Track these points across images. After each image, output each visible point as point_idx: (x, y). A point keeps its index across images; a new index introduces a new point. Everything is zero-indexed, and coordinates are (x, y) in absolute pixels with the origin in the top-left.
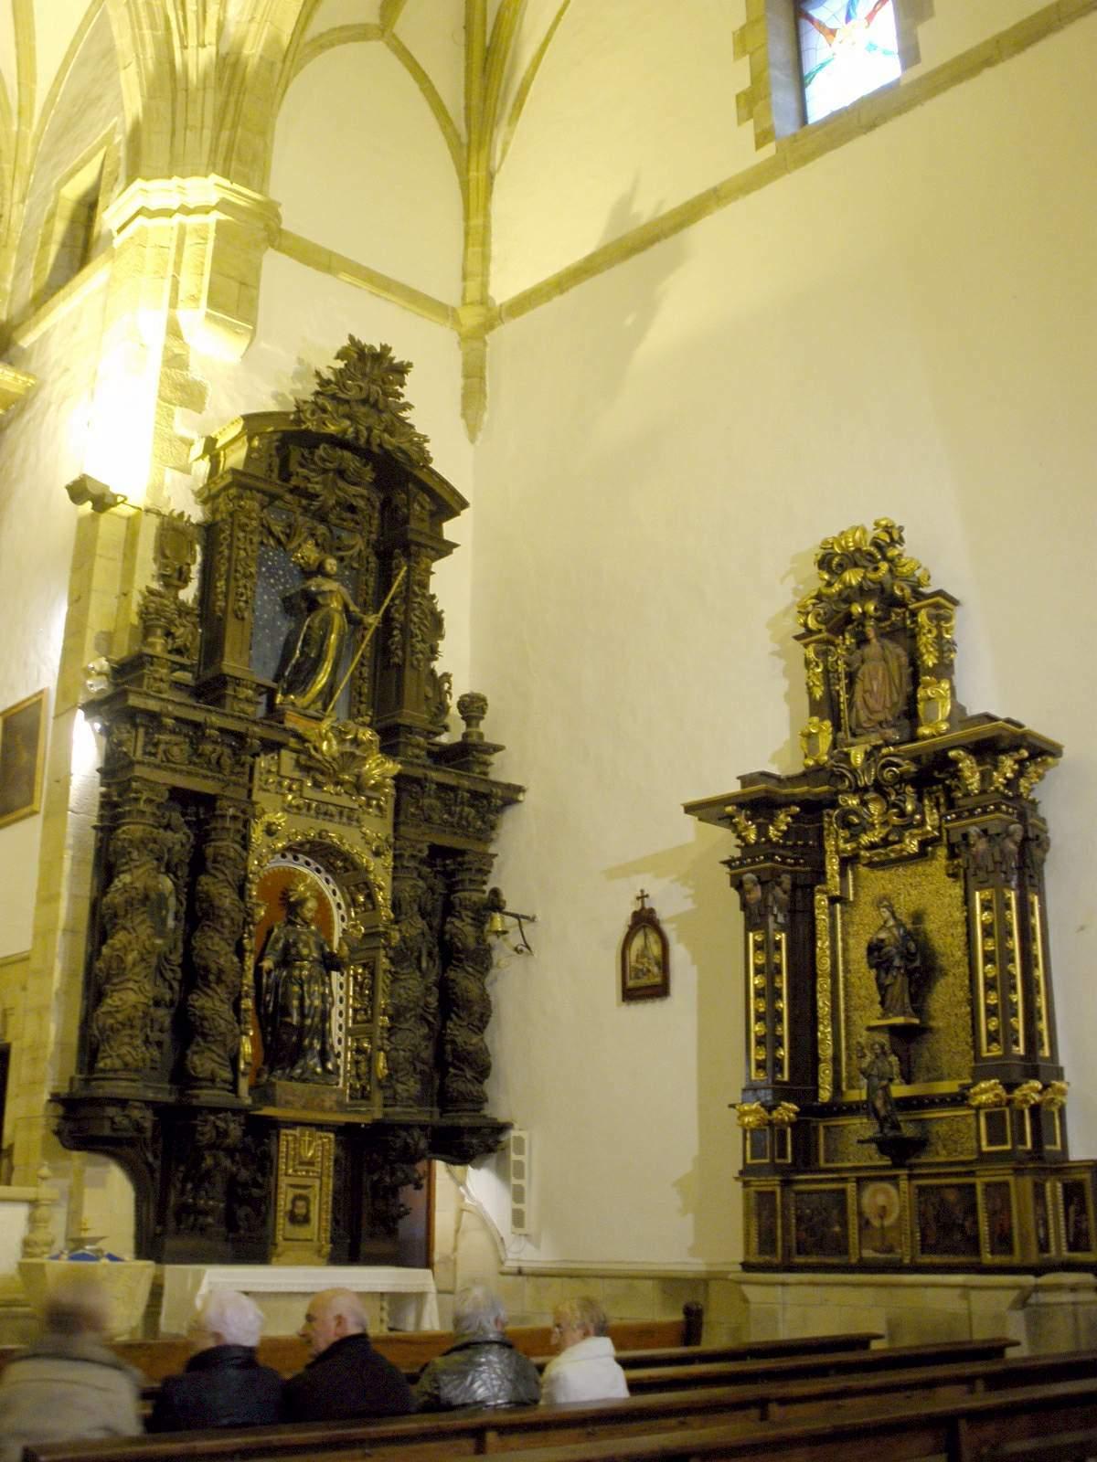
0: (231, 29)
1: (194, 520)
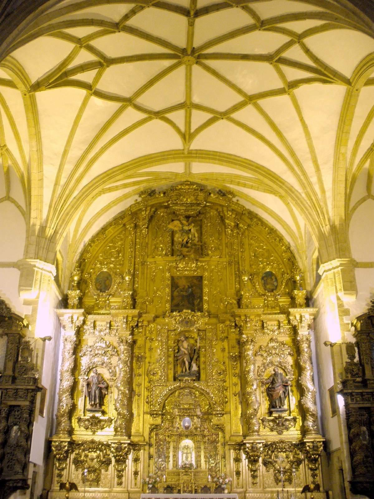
0: (331, 218)
1: (353, 343)
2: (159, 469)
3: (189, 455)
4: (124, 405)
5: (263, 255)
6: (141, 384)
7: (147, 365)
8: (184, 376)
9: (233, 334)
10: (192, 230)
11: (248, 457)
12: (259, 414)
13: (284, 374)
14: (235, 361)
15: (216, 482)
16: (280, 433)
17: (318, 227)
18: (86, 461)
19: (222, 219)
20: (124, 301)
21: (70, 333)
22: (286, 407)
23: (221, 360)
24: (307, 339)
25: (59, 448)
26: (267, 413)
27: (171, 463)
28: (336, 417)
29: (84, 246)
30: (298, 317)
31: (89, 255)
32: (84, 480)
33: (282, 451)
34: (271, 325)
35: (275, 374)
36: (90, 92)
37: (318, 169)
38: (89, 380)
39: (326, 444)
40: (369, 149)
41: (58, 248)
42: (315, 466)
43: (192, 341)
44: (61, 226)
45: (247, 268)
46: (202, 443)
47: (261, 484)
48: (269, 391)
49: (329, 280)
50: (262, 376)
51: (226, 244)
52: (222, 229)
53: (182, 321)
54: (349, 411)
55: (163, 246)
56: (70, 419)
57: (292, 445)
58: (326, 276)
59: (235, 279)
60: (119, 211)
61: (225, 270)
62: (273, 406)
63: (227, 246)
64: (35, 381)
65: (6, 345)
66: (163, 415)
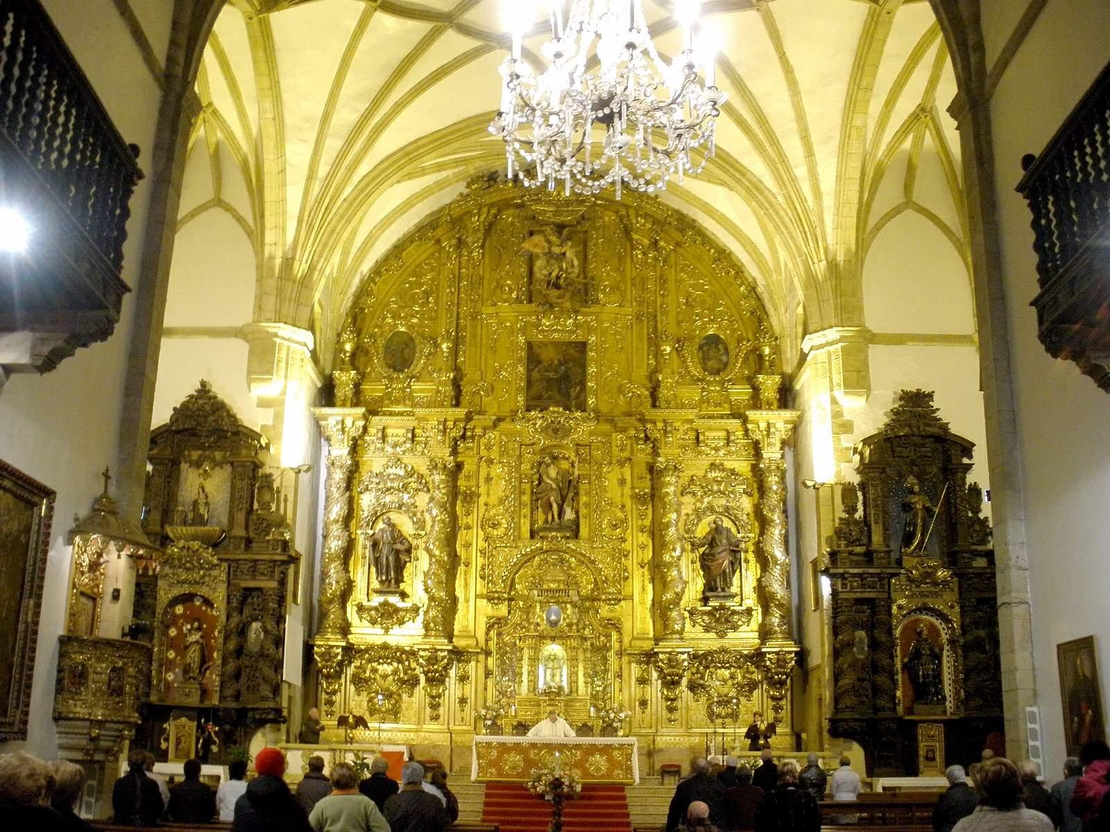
0: (831, 247)
2: (503, 693)
3: (557, 672)
4: (442, 582)
5: (703, 302)
6: (471, 544)
7: (482, 509)
8: (550, 530)
9: (642, 454)
10: (568, 254)
11: (663, 676)
12: (683, 603)
13: (734, 530)
14: (643, 505)
15: (603, 718)
16: (722, 635)
17: (805, 263)
18: (375, 679)
19: (627, 231)
20: (438, 391)
21: (341, 451)
22: (734, 589)
23: (618, 500)
24: (778, 468)
25: (328, 656)
26: (700, 600)
27: (525, 683)
28: (818, 612)
29: (361, 281)
30: (763, 426)
31: (371, 301)
32: (373, 711)
33: (723, 667)
34: (714, 436)
35: (717, 530)
36: (374, 5)
37: (809, 153)
38: (375, 536)
39: (802, 656)
40: (912, 114)
41: (317, 296)
42: (781, 693)
43: (565, 465)
44: (320, 257)
45: (672, 329)
46: (580, 652)
47: (684, 723)
48: (704, 559)
49: (819, 366)
50: (693, 532)
51: (633, 279)
52: (625, 251)
53: (547, 427)
54: (837, 603)
55: (512, 286)
56: (344, 607)
57: (741, 656)
58: (815, 358)
59: (649, 349)
60: (428, 212)
61: (630, 330)
62: (710, 587)
63: (633, 285)
64: (285, 545)
65: (229, 480)
66: (511, 599)
